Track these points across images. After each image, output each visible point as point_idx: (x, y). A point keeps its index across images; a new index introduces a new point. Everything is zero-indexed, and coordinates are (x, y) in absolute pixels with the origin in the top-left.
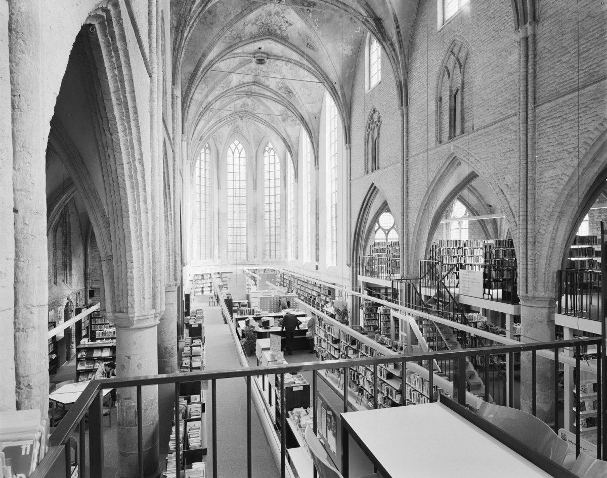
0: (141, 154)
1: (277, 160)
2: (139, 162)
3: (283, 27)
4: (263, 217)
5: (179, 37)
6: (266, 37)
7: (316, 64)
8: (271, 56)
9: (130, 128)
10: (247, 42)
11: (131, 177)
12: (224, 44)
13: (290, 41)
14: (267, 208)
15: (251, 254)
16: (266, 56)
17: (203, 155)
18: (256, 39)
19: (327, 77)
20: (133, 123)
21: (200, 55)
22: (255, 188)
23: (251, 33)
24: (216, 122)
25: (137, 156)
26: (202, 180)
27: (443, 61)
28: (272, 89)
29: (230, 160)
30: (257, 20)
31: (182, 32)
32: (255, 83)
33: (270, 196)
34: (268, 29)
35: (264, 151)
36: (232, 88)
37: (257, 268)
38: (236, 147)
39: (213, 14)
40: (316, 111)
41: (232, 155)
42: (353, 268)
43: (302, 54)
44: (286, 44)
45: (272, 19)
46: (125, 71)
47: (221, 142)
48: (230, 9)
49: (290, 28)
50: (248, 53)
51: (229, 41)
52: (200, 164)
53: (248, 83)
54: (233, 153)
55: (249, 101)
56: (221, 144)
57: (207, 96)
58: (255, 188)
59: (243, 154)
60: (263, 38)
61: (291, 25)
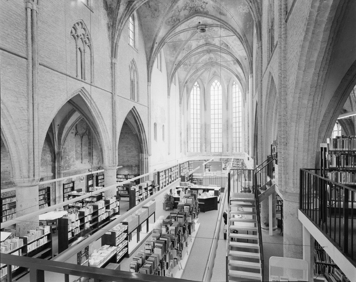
3: (203, 6)
4: (232, 126)
5: (114, 30)
6: (195, 15)
7: (227, 24)
10: (183, 21)
12: (170, 26)
14: (234, 121)
15: (225, 149)
16: (204, 26)
17: (195, 91)
21: (154, 36)
22: (227, 108)
28: (217, 46)
29: (212, 93)
30: (186, 7)
31: (115, 27)
32: (207, 44)
34: (195, 10)
35: (233, 85)
36: (193, 50)
37: (228, 158)
38: (216, 84)
39: (158, 11)
41: (217, 89)
43: (219, 20)
48: (166, 5)
50: (192, 28)
51: (172, 24)
53: (202, 45)
54: (214, 88)
55: (212, 55)
57: (176, 58)
58: (227, 108)
59: (220, 88)
61: (207, 3)
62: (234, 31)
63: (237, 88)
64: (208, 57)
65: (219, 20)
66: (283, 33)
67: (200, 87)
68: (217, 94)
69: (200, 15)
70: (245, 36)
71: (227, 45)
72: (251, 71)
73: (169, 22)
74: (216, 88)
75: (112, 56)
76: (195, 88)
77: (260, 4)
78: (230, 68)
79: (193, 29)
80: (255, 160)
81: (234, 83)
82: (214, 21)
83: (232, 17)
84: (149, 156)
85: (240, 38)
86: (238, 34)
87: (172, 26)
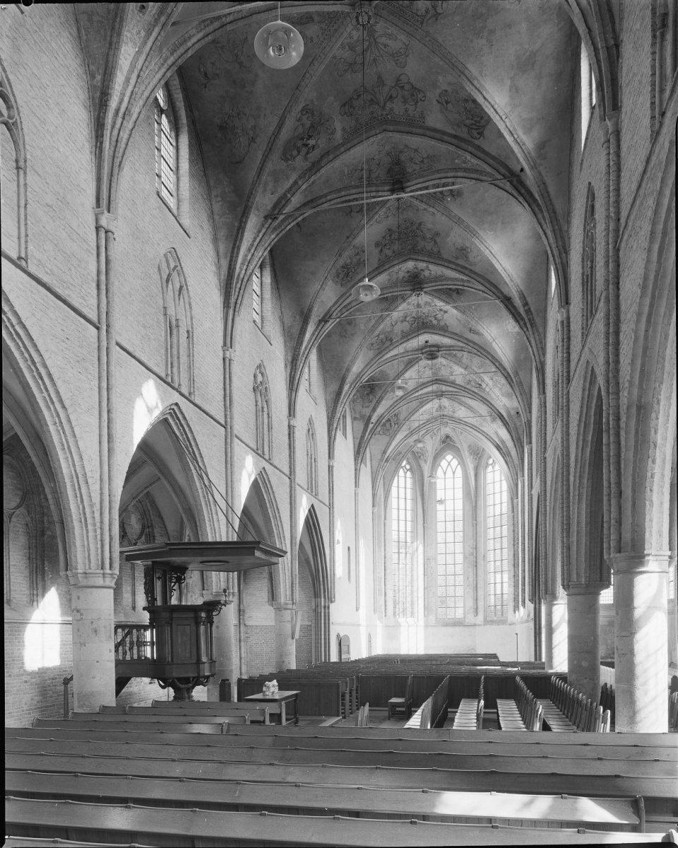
3: (439, 315)
12: (372, 351)
13: (450, 329)
16: (436, 349)
17: (402, 480)
23: (403, 331)
26: (400, 512)
28: (459, 385)
30: (406, 317)
32: (437, 381)
33: (454, 521)
39: (353, 325)
42: (535, 603)
45: (424, 311)
46: (189, 435)
47: (425, 460)
49: (446, 316)
51: (377, 347)
59: (459, 472)
61: (446, 312)
62: (497, 364)
63: (497, 474)
64: (436, 406)
66: (565, 404)
67: (411, 470)
68: (443, 487)
69: (431, 331)
70: (517, 373)
71: (480, 385)
72: (528, 440)
73: (372, 344)
74: (449, 473)
75: (290, 415)
76: (401, 472)
77: (542, 336)
80: (535, 605)
81: (491, 461)
83: (494, 340)
84: (332, 602)
85: (507, 377)
86: (505, 369)
87: (377, 352)
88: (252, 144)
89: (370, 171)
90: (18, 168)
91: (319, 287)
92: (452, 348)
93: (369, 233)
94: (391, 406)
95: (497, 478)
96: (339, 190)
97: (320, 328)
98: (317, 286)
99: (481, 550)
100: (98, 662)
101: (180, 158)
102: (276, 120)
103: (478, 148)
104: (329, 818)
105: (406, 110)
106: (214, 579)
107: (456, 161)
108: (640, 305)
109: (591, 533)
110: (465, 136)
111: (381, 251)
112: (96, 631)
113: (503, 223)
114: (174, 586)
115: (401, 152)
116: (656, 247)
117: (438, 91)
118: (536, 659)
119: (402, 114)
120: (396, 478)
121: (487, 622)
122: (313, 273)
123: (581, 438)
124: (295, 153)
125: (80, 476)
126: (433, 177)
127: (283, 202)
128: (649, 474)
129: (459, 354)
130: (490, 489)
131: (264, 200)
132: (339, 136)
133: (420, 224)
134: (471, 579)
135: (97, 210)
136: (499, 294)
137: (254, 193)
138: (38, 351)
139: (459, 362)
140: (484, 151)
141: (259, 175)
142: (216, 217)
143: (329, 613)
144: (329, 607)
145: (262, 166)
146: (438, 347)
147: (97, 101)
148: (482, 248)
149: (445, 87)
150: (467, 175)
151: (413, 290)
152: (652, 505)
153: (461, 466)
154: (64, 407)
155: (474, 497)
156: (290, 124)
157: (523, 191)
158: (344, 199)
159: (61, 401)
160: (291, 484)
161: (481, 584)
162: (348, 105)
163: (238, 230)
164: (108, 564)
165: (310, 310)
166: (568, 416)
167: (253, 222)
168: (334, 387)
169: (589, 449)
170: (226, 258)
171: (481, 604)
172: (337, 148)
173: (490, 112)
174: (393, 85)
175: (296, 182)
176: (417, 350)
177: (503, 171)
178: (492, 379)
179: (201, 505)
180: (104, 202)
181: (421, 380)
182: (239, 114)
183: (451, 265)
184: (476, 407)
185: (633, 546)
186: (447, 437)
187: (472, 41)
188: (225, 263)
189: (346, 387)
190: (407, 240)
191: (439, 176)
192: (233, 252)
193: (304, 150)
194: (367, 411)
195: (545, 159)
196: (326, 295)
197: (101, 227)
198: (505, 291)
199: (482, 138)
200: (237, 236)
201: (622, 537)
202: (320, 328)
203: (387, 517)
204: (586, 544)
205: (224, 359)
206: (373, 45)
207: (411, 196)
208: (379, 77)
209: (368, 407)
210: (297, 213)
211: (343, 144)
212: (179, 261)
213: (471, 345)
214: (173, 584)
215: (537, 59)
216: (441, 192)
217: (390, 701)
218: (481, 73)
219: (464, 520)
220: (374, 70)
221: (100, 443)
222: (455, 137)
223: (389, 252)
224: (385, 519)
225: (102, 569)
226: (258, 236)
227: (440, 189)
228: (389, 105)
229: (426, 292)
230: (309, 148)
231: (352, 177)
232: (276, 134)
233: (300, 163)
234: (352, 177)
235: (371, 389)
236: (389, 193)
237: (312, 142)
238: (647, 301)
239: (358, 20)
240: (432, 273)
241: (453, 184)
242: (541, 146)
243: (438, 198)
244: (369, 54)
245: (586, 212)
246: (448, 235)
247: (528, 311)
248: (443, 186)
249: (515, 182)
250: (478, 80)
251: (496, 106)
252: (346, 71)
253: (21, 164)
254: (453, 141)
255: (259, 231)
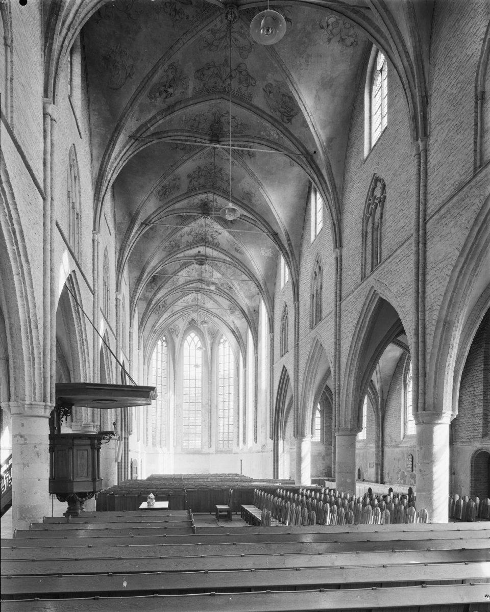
0: (86, 336)
1: (231, 352)
2: (86, 341)
3: (214, 235)
8: (210, 257)
9: (80, 323)
11: (81, 348)
13: (220, 246)
17: (159, 347)
18: (192, 247)
19: (254, 276)
20: (82, 321)
24: (170, 316)
25: (84, 337)
27: (314, 267)
29: (186, 352)
32: (201, 281)
34: (202, 238)
38: (193, 340)
39: (154, 230)
40: (254, 304)
42: (274, 440)
43: (232, 257)
44: (218, 249)
51: (169, 250)
52: (157, 356)
54: (189, 346)
55: (199, 296)
56: (178, 337)
60: (198, 245)
61: (220, 234)
65: (232, 257)
67: (166, 341)
68: (194, 356)
70: (265, 284)
77: (298, 263)
78: (224, 318)
79: (190, 258)
80: (274, 441)
81: (222, 341)
82: (220, 254)
84: (130, 434)
87: (168, 253)
88: (129, 78)
89: (199, 122)
90: (6, 45)
91: (146, 198)
92: (217, 260)
93: (188, 166)
94: (166, 293)
95: (227, 353)
96: (177, 131)
97: (142, 229)
98: (144, 197)
99: (214, 402)
100: (39, 480)
101: (74, 72)
102: (150, 67)
103: (286, 129)
104: (207, 595)
105: (240, 89)
106: (83, 414)
107: (262, 133)
108: (458, 261)
109: (355, 396)
110: (278, 118)
111: (191, 181)
112: (38, 454)
113: (279, 182)
114: (62, 417)
115: (222, 115)
116: (477, 229)
117: (266, 83)
118: (274, 478)
119: (236, 90)
120: (156, 348)
121: (218, 452)
122: (142, 187)
123: (356, 335)
124: (158, 94)
125: (32, 321)
126: (243, 139)
127: (144, 129)
128: (447, 364)
129: (219, 264)
130: (221, 359)
131: (131, 125)
132: (190, 91)
133: (221, 169)
134: (207, 421)
135: (45, 99)
136: (270, 230)
137: (126, 116)
138: (16, 209)
139: (219, 270)
140: (290, 133)
141: (132, 103)
142: (93, 127)
143: (128, 442)
144: (128, 439)
145: (136, 97)
146: (207, 257)
147: (48, 8)
148: (265, 196)
149: (271, 81)
150: (269, 144)
151: (203, 214)
152: (447, 383)
153: (201, 341)
154: (27, 261)
155: (210, 364)
156: (160, 72)
157: (314, 166)
158: (178, 138)
159: (26, 255)
160: (117, 343)
161: (213, 425)
162: (200, 72)
163: (110, 141)
164: (49, 397)
165: (137, 214)
166: (340, 319)
167: (122, 139)
168: (136, 274)
169: (361, 343)
170: (98, 160)
171: (213, 439)
172: (188, 100)
173: (302, 108)
174: (234, 68)
175: (154, 117)
176: (192, 256)
177: (301, 149)
178: (239, 285)
179: (78, 354)
180: (50, 94)
181: (189, 278)
182: (121, 52)
183: (238, 203)
184: (220, 302)
185: (434, 407)
186: (193, 320)
187: (296, 57)
188: (97, 165)
189: (145, 275)
190: (211, 180)
191: (247, 139)
192: (104, 158)
193: (164, 95)
194: (150, 295)
195: (331, 149)
196: (149, 206)
197: (48, 114)
198: (275, 228)
199: (290, 123)
200: (109, 146)
201: (426, 401)
202: (142, 229)
203: (149, 373)
204: (352, 403)
205: (93, 241)
206: (228, 36)
207: (223, 148)
208: (226, 60)
209: (150, 292)
210: (147, 140)
211: (192, 99)
212: (76, 156)
213: (235, 260)
214: (61, 416)
215: (334, 83)
216: (242, 151)
217: (242, 505)
218: (299, 80)
219: (202, 380)
220: (224, 54)
221: (44, 295)
222: (271, 117)
223: (196, 184)
224: (148, 375)
225: (44, 401)
226: (123, 150)
227: (242, 149)
228: (228, 81)
229: (211, 217)
230: (168, 95)
231: (187, 123)
232: (149, 78)
233: (159, 103)
234: (187, 123)
235: (156, 280)
236: (208, 142)
237: (171, 90)
238: (463, 260)
239: (227, 16)
240: (218, 204)
241: (250, 147)
242: (330, 140)
243: (239, 155)
244: (223, 42)
245: (369, 191)
246: (239, 181)
247: (290, 245)
248: (244, 147)
249: (309, 159)
250: (297, 85)
251: (306, 106)
252: (205, 47)
253: (9, 42)
254: (270, 119)
255: (124, 147)
